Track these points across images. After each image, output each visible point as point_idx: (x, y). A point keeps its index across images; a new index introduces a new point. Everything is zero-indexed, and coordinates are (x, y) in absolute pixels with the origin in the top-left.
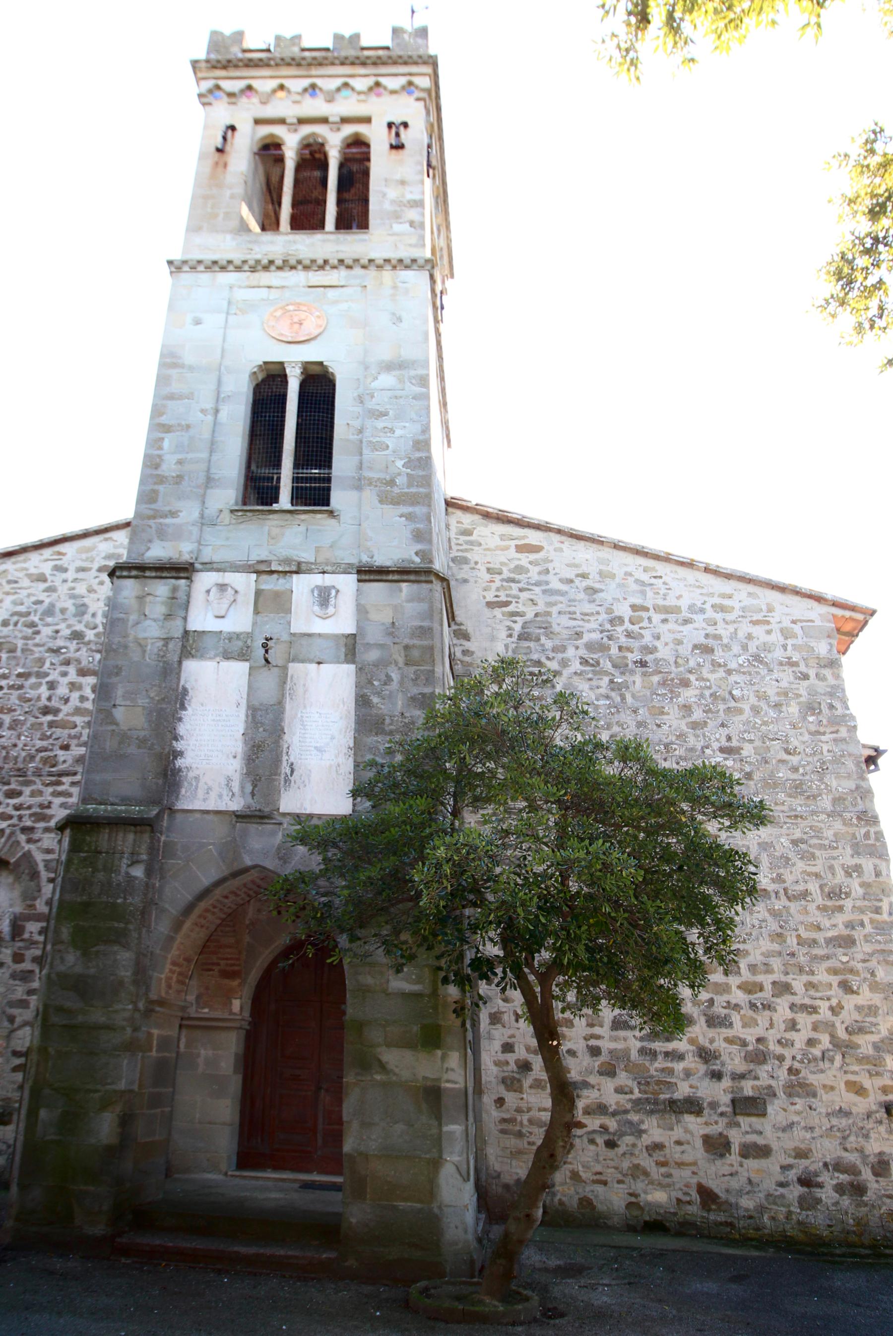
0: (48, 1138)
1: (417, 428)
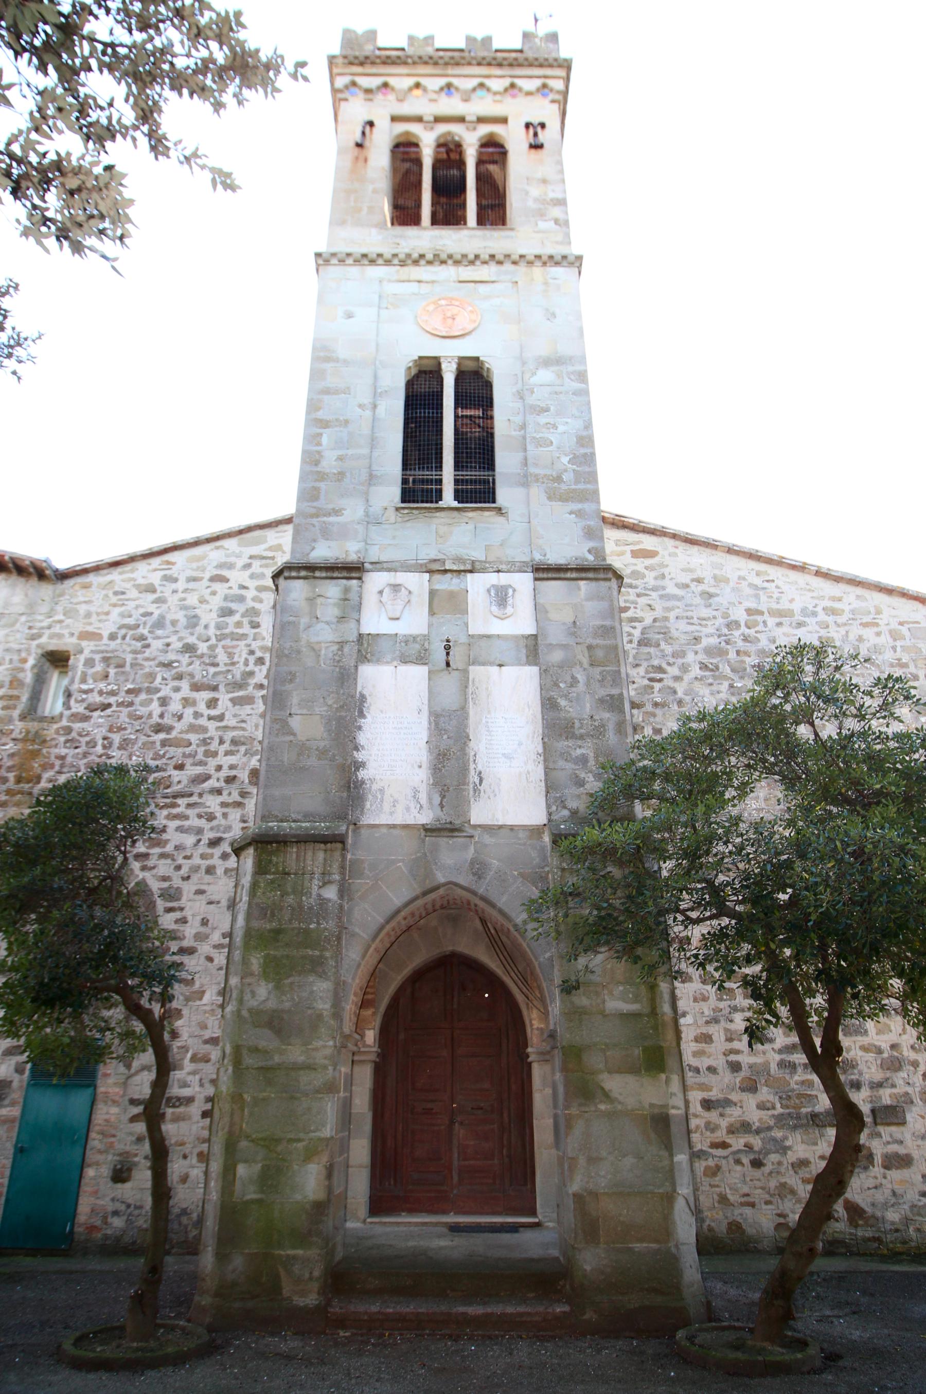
0: (248, 1197)
1: (579, 424)
